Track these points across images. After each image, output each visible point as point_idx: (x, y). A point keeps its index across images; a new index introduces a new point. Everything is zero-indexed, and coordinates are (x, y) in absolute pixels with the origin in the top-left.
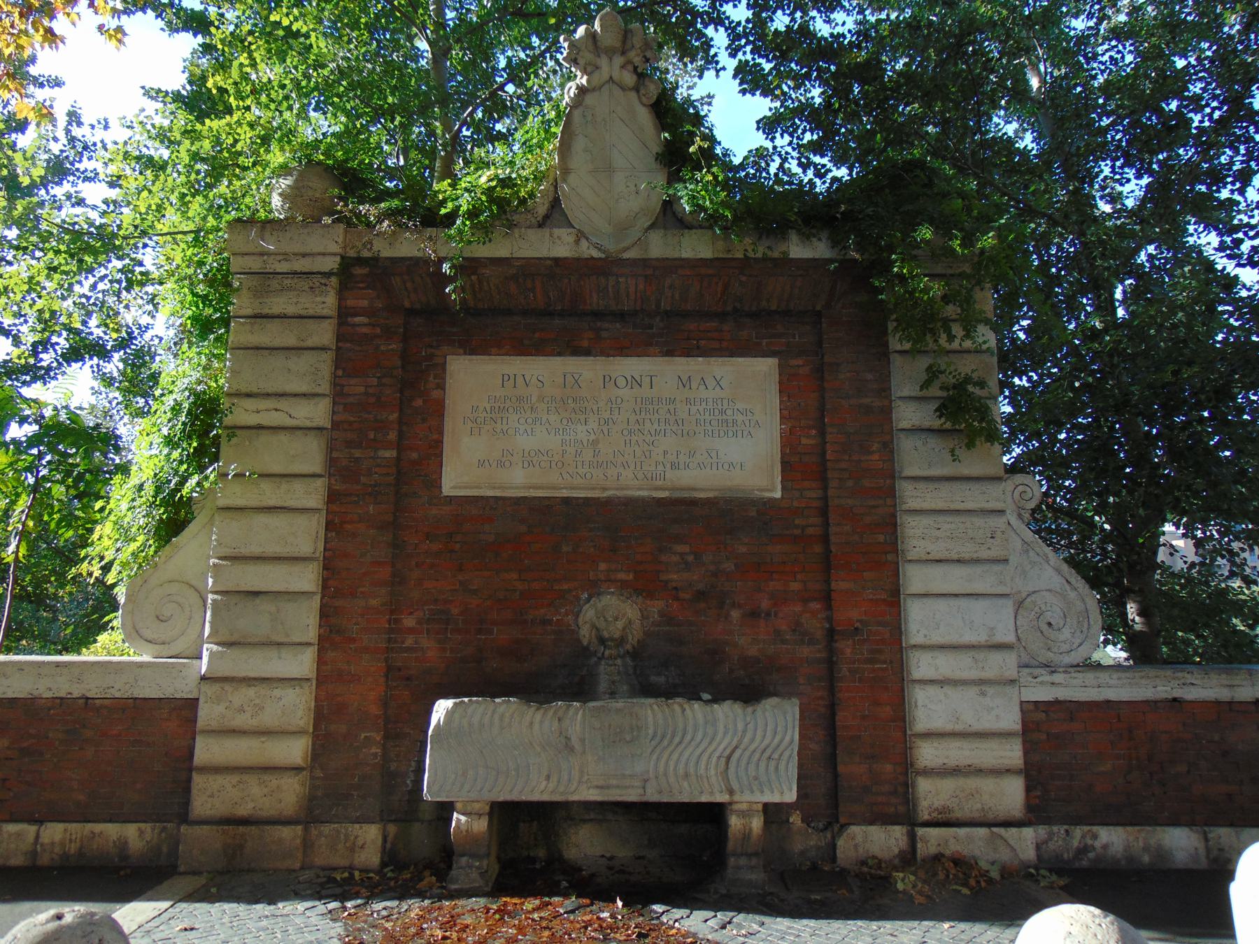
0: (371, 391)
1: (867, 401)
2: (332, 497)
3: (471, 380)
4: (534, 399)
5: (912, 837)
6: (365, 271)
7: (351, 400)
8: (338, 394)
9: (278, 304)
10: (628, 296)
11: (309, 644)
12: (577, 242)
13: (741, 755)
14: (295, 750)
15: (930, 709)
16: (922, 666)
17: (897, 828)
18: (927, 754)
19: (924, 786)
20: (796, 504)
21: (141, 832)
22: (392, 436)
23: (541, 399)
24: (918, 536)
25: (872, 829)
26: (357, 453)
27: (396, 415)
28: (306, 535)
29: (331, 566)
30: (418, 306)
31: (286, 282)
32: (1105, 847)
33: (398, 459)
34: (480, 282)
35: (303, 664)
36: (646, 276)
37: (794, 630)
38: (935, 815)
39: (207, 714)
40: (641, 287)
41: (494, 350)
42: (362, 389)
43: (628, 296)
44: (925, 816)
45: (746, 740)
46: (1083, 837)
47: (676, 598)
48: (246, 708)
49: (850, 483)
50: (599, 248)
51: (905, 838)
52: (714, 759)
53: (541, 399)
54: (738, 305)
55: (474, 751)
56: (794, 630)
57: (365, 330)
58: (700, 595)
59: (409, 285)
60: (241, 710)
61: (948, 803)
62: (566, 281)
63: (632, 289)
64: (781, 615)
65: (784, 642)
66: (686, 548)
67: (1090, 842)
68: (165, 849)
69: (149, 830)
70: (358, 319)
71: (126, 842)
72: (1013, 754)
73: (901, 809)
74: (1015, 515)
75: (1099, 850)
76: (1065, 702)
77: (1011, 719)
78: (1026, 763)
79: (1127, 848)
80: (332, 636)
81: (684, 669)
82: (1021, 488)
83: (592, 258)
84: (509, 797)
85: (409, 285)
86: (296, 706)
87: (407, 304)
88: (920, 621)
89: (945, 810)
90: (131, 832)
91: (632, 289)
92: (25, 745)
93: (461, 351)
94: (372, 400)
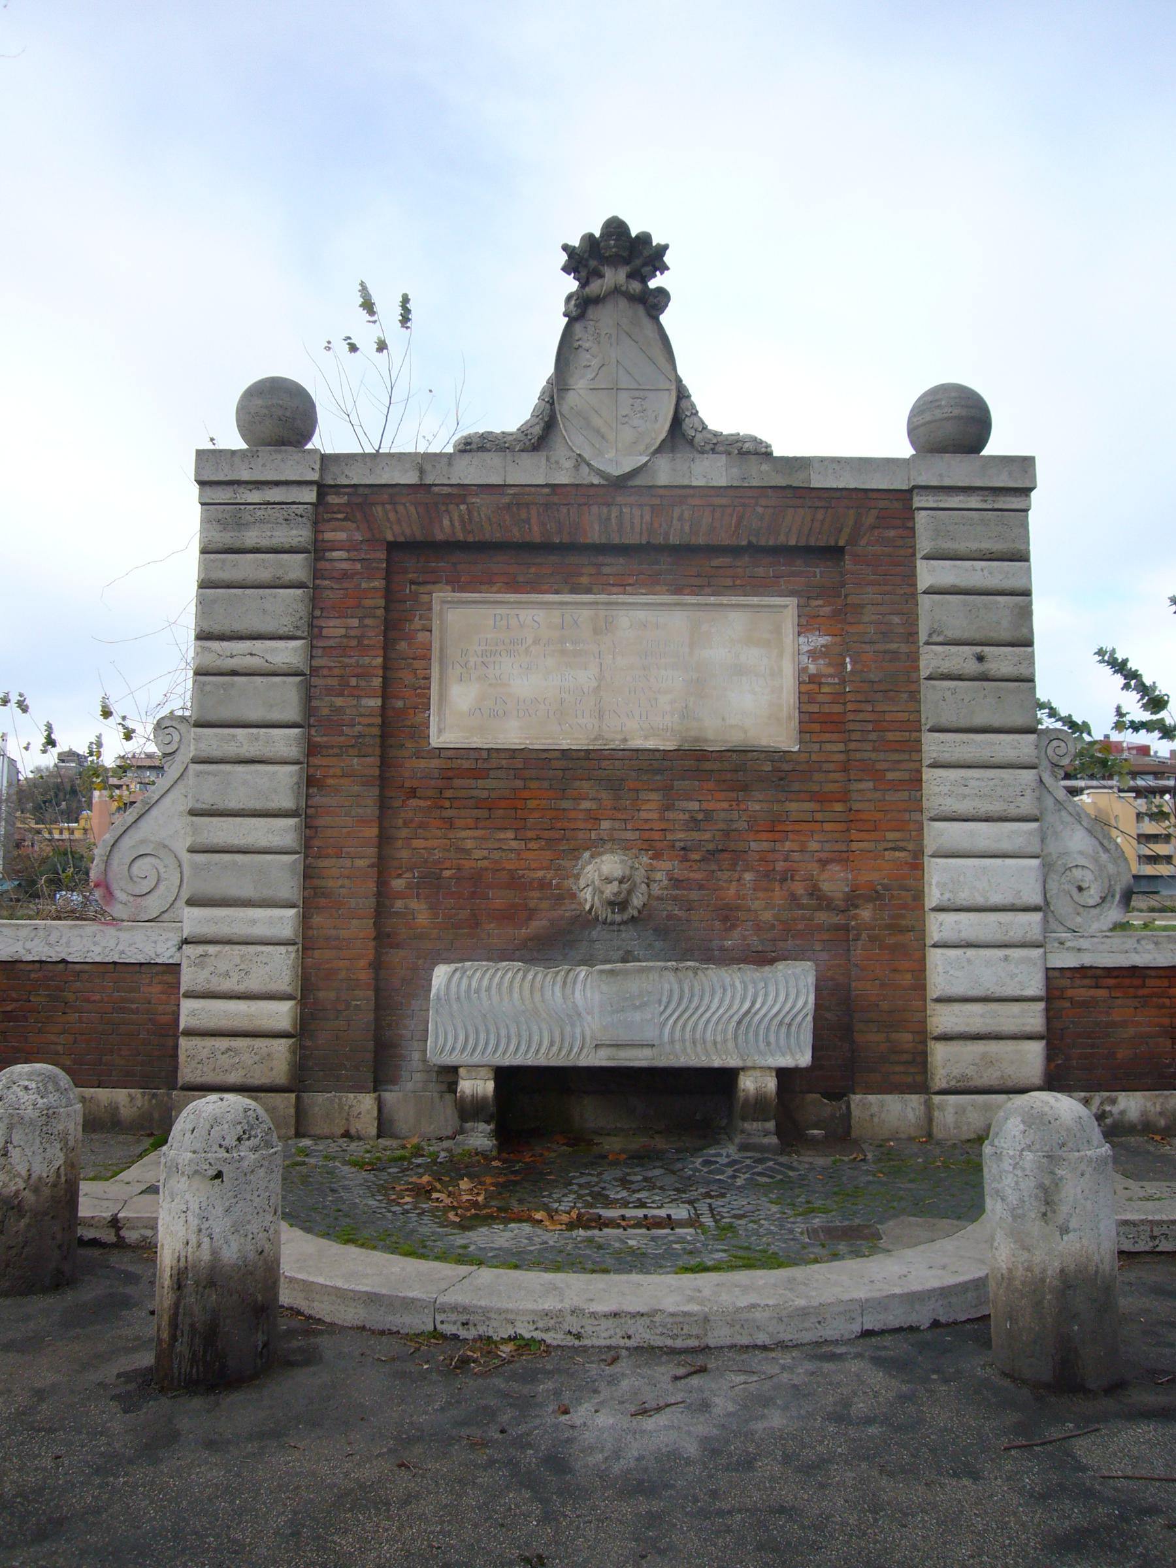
0: (352, 633)
1: (894, 646)
2: (312, 749)
3: (1134, 897)
4: (530, 641)
5: (929, 1108)
6: (344, 500)
7: (331, 643)
8: (313, 632)
9: (252, 537)
10: (632, 527)
11: (938, 1000)
12: (577, 467)
13: (751, 1018)
14: (281, 1014)
15: (944, 972)
16: (939, 926)
17: (914, 1097)
18: (943, 1019)
19: (939, 1053)
20: (814, 757)
21: (132, 1098)
22: (377, 682)
23: (536, 641)
24: (940, 789)
25: (888, 1098)
26: (339, 702)
27: (380, 660)
28: (280, 785)
29: (308, 818)
30: (402, 539)
31: (259, 513)
32: (1122, 1113)
33: (383, 707)
34: (469, 511)
35: (284, 922)
36: (652, 506)
37: (811, 894)
38: (953, 1083)
39: (188, 978)
40: (647, 518)
41: (484, 587)
42: (342, 631)
43: (632, 527)
44: (937, 1089)
45: (758, 1006)
46: (1102, 1103)
47: (685, 859)
48: (231, 974)
49: (873, 736)
50: (599, 473)
51: (922, 1107)
52: (773, 1028)
53: (536, 641)
54: (754, 540)
55: (487, 1014)
56: (811, 894)
57: (344, 565)
58: (712, 855)
59: (392, 516)
60: (227, 975)
61: (967, 1071)
62: (565, 511)
63: (637, 521)
64: (797, 878)
65: (800, 907)
66: (695, 806)
67: (1108, 1108)
68: (156, 1115)
69: (139, 1096)
70: (336, 554)
71: (117, 1108)
72: (1033, 1018)
73: (918, 1078)
74: (1048, 772)
75: (1116, 1116)
76: (1091, 968)
77: (1035, 985)
78: (1048, 1029)
79: (1144, 1113)
80: (313, 898)
81: (674, 931)
82: (1055, 743)
83: (593, 485)
84: (518, 1061)
85: (392, 516)
86: (278, 968)
87: (390, 538)
88: (940, 879)
89: (964, 1077)
90: (120, 1096)
91: (637, 521)
92: (9, 1008)
93: (449, 588)
94: (354, 643)
